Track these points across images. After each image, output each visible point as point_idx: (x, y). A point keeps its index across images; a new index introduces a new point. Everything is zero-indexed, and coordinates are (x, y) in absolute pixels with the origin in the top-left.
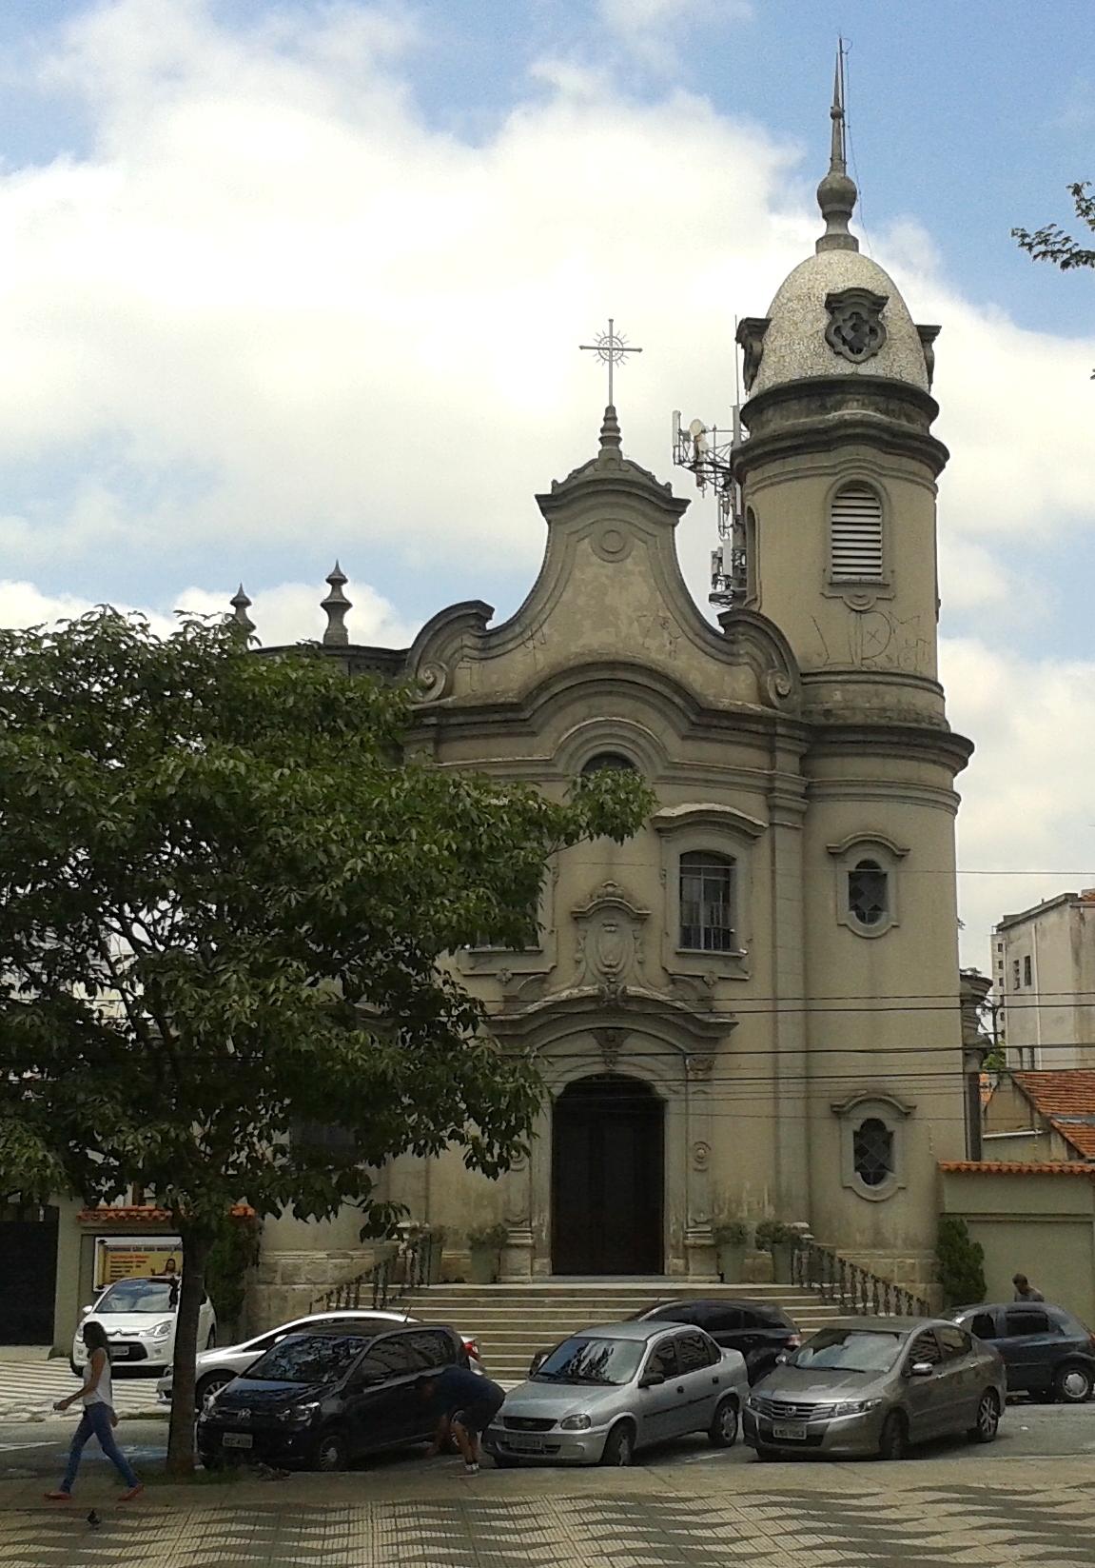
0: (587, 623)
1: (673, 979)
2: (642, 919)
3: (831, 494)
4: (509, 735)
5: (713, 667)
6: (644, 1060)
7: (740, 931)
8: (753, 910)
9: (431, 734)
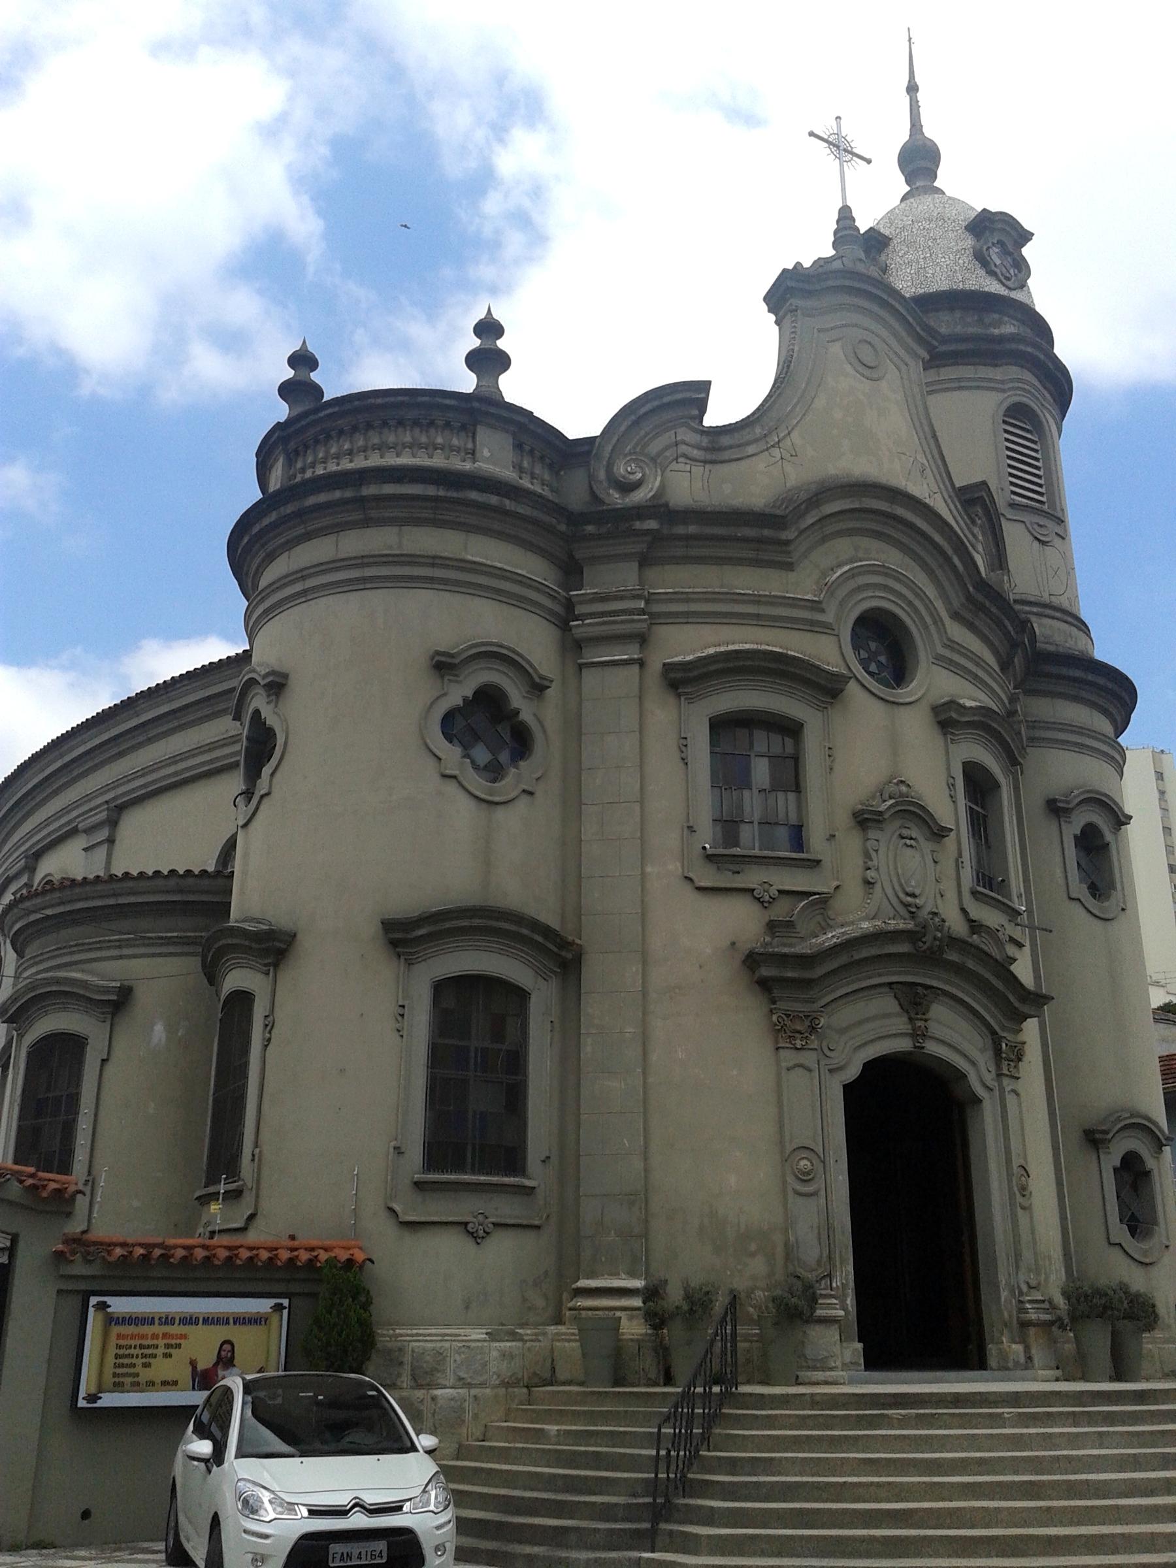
3: (1001, 412)
6: (954, 1038)
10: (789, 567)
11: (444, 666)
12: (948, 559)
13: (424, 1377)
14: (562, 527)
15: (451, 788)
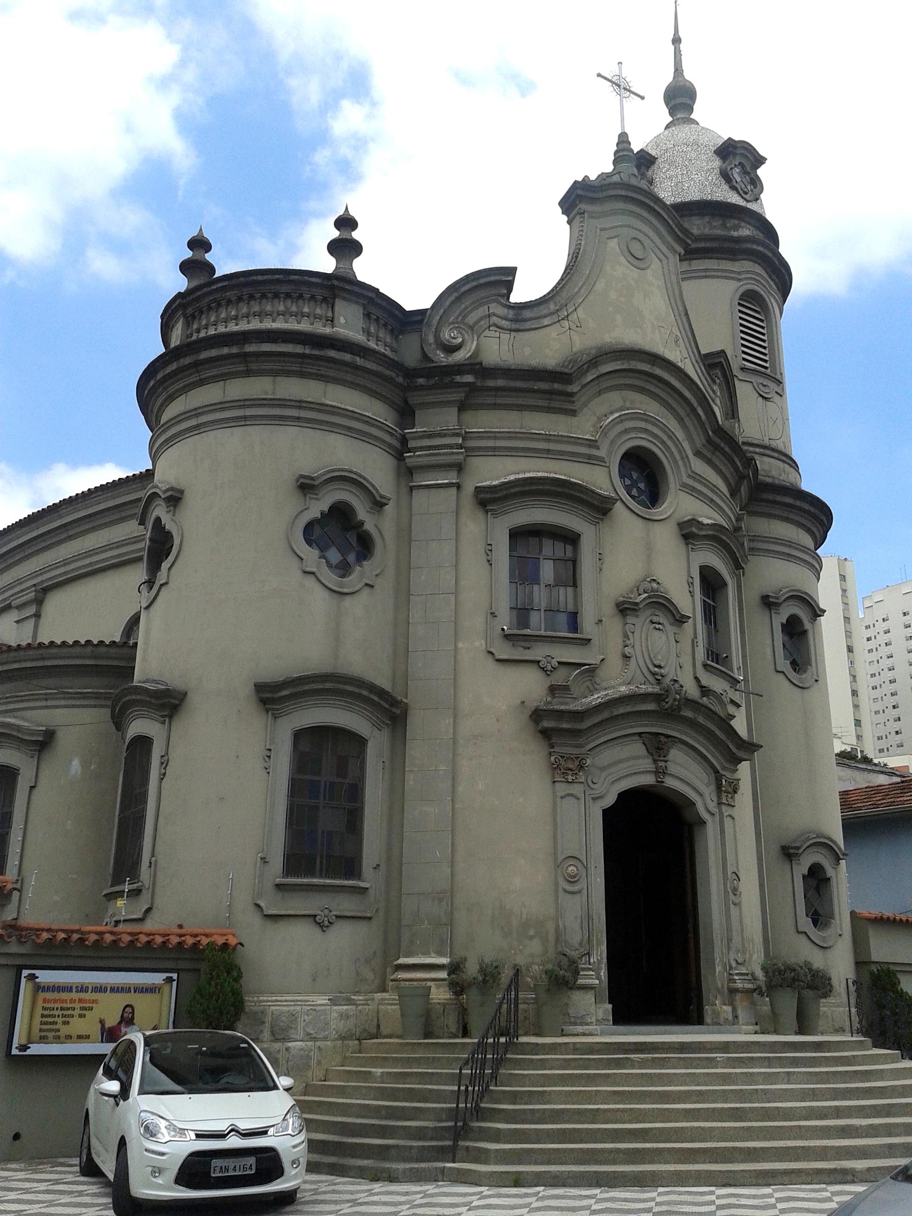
0: (619, 318)
3: (738, 296)
4: (550, 410)
6: (686, 775)
10: (573, 413)
11: (306, 487)
12: (693, 410)
14: (400, 380)
15: (310, 582)
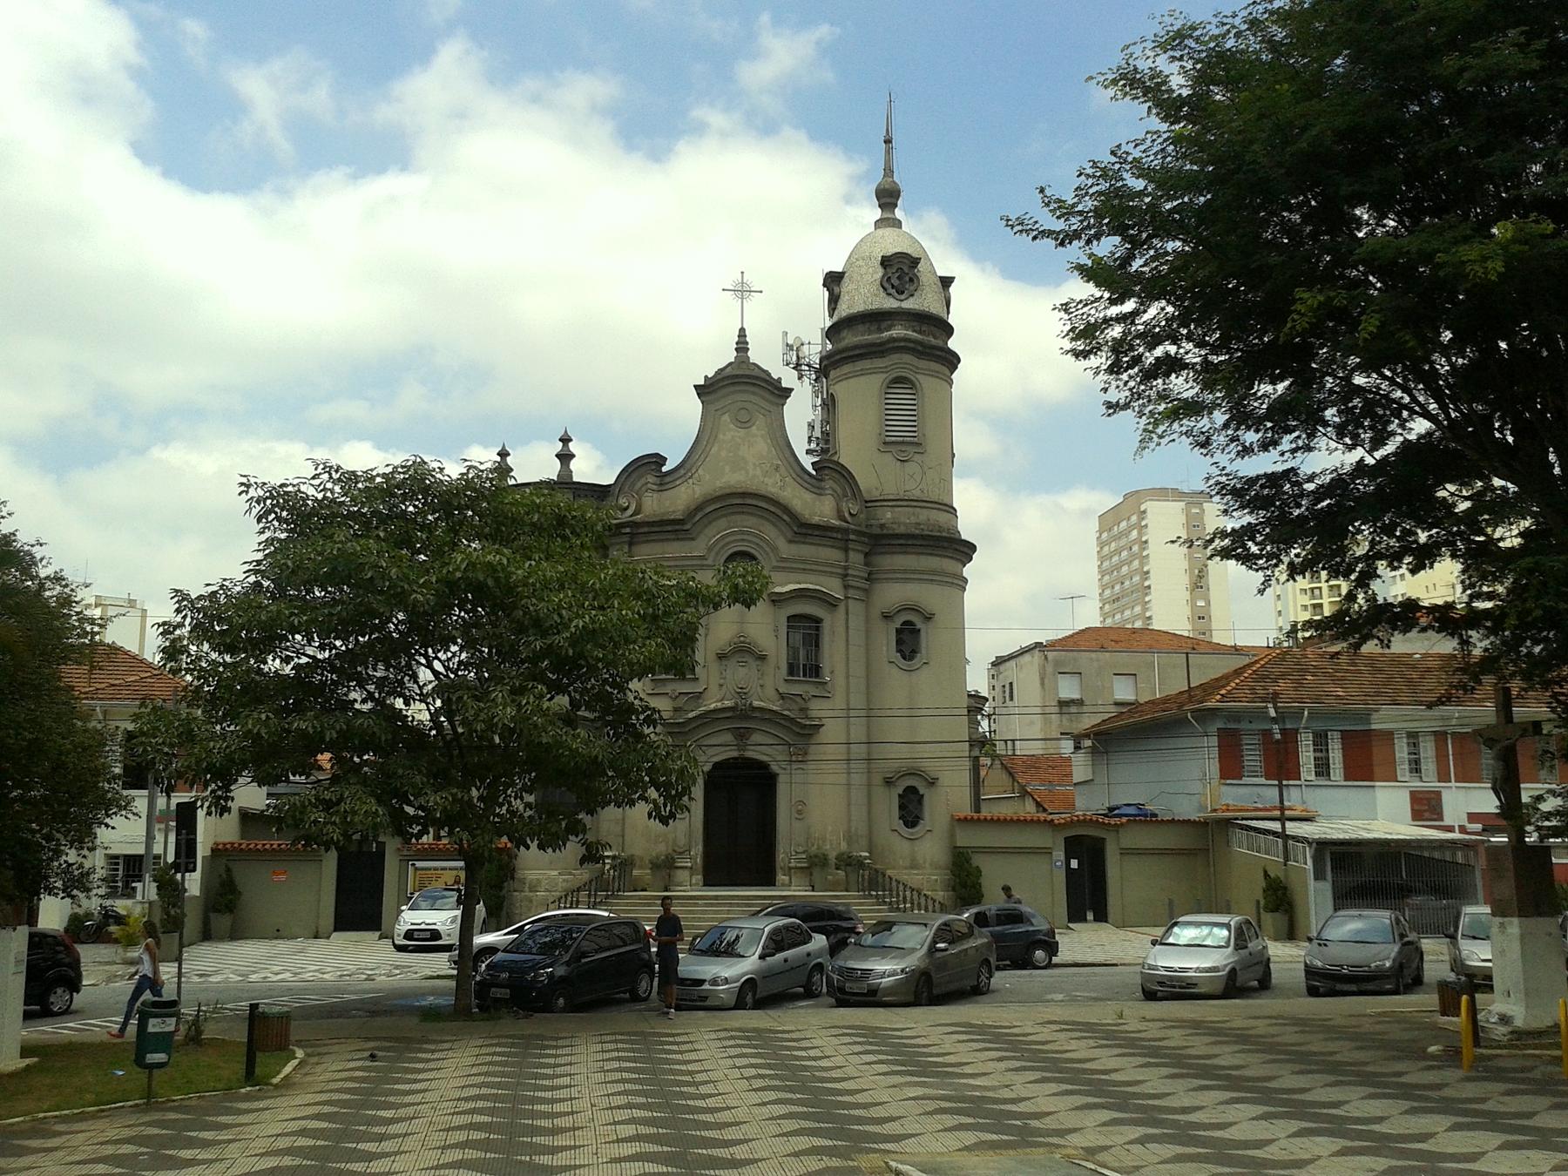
0: (727, 469)
1: (782, 697)
2: (762, 658)
5: (808, 496)
6: (763, 748)
7: (826, 666)
8: (833, 654)
9: (626, 539)
13: (533, 889)
